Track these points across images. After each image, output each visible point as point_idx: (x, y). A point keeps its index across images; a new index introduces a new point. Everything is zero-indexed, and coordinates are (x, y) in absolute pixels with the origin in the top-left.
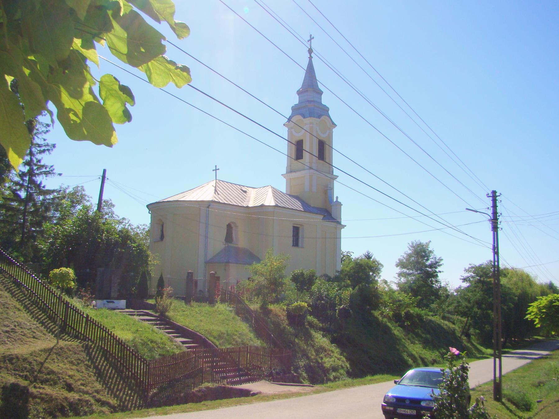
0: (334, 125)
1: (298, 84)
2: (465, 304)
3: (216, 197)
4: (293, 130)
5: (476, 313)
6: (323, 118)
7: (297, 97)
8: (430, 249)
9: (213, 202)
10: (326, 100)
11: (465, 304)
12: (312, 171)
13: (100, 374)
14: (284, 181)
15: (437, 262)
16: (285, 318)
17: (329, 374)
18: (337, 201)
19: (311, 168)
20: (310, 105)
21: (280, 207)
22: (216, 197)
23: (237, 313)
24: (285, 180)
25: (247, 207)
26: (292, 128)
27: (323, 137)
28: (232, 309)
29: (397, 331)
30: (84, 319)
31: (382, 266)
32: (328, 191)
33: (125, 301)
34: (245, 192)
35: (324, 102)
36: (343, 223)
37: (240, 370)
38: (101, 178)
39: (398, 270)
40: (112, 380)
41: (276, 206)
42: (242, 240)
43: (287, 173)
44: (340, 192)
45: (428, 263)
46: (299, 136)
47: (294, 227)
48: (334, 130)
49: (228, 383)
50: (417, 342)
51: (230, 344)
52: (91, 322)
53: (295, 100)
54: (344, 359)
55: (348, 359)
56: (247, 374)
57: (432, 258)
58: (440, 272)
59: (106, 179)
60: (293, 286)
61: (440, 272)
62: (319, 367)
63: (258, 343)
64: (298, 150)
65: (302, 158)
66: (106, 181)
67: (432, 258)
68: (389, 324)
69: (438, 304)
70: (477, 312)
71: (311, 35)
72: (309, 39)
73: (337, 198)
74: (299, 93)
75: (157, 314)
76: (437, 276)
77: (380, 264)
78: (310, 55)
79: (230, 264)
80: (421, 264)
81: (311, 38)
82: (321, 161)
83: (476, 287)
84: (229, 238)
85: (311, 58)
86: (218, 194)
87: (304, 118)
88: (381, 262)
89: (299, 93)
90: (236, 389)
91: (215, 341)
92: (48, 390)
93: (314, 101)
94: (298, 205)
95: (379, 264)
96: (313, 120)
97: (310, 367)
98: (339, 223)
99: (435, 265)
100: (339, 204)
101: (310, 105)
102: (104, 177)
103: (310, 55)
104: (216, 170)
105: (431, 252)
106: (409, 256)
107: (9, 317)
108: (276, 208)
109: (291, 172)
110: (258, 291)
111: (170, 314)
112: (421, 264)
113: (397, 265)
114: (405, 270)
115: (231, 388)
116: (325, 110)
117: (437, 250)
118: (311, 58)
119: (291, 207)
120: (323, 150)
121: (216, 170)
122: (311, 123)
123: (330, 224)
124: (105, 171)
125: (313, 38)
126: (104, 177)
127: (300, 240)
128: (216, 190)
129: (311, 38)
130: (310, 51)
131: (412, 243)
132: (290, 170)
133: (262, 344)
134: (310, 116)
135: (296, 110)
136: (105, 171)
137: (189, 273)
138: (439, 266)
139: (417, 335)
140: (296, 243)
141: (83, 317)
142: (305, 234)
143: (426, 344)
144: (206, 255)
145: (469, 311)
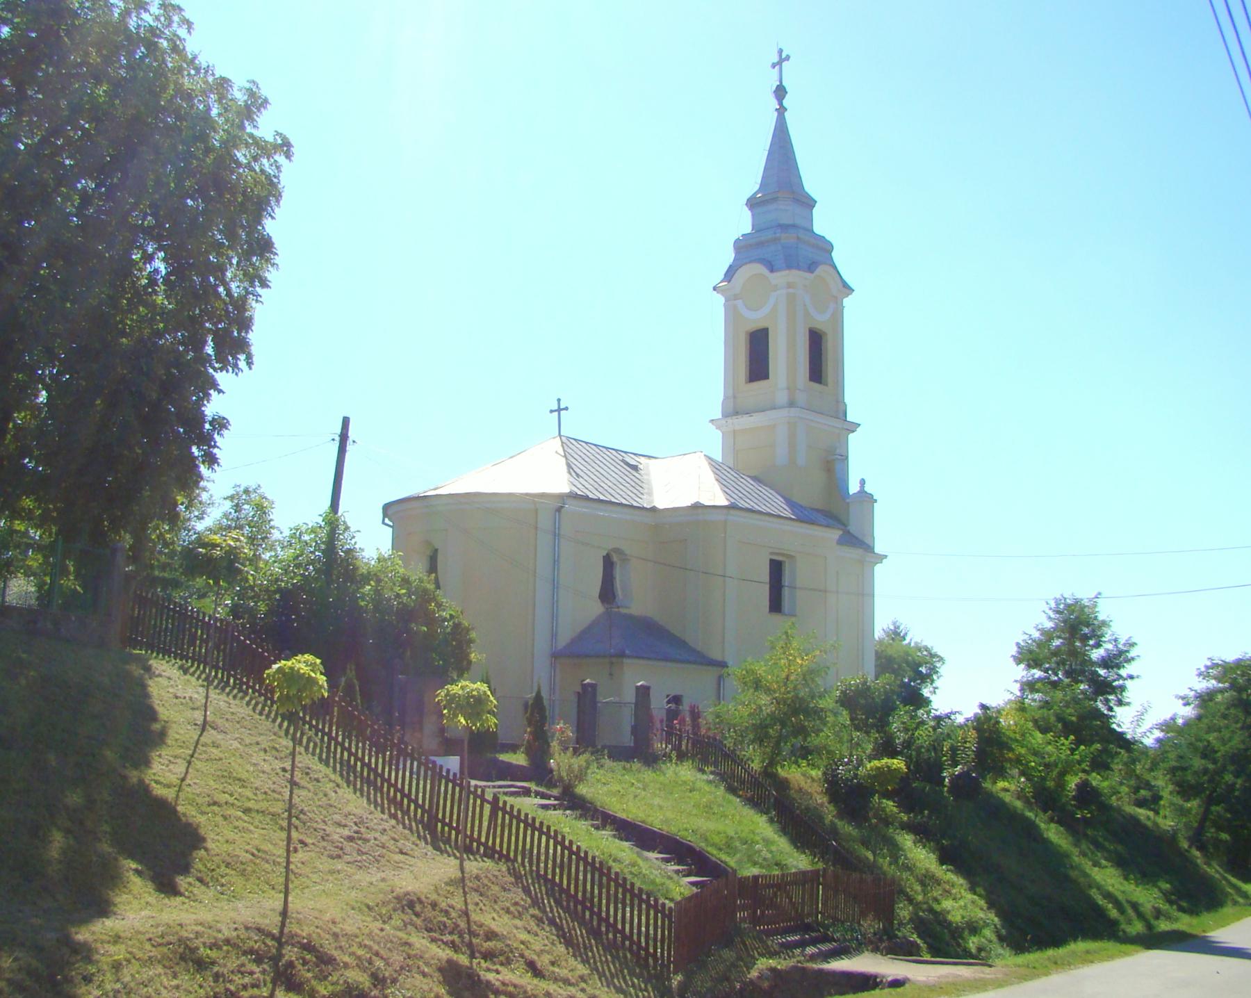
0: (847, 289)
1: (751, 183)
2: (1198, 763)
3: (576, 483)
4: (739, 303)
5: (1231, 787)
6: (821, 270)
7: (747, 215)
8: (1101, 617)
9: (573, 496)
10: (823, 223)
11: (1198, 763)
12: (794, 412)
13: (569, 942)
14: (717, 436)
15: (1121, 653)
16: (825, 799)
17: (963, 939)
18: (862, 492)
19: (792, 404)
20: (783, 237)
21: (741, 509)
22: (576, 483)
23: (732, 790)
24: (719, 434)
25: (654, 509)
26: (736, 297)
27: (821, 320)
28: (712, 777)
29: (1054, 834)
30: (487, 808)
31: (941, 659)
32: (833, 464)
33: (458, 758)
34: (635, 468)
35: (818, 228)
36: (879, 548)
37: (807, 928)
38: (337, 439)
39: (1020, 672)
40: (592, 951)
41: (733, 507)
42: (639, 598)
43: (726, 415)
44: (864, 466)
45: (1096, 654)
46: (756, 319)
47: (771, 561)
48: (846, 301)
49: (812, 958)
50: (1104, 862)
51: (755, 864)
52: (505, 812)
53: (743, 223)
54: (982, 903)
55: (991, 905)
56: (826, 939)
57: (1109, 641)
58: (1131, 677)
59: (350, 442)
60: (845, 717)
61: (1131, 677)
62: (940, 923)
63: (800, 862)
64: (755, 356)
65: (766, 377)
66: (349, 447)
67: (1109, 641)
68: (1030, 815)
69: (1125, 764)
70: (1234, 784)
71: (780, 51)
72: (776, 60)
73: (863, 482)
74: (752, 203)
75: (555, 792)
76: (1122, 688)
77: (936, 655)
78: (781, 104)
79: (626, 661)
80: (1074, 657)
81: (782, 60)
82: (816, 386)
83: (1225, 716)
84: (607, 593)
85: (781, 110)
86: (578, 475)
87: (772, 271)
88: (937, 649)
89: (752, 203)
90: (833, 974)
91: (724, 857)
92: (507, 975)
93: (794, 226)
94: (777, 505)
95: (932, 656)
96: (796, 276)
97: (921, 920)
98: (869, 548)
99: (1114, 661)
100: (866, 499)
101: (783, 237)
102: (344, 437)
103: (781, 104)
104: (559, 410)
105: (1104, 623)
106: (1048, 635)
107: (331, 802)
108: (732, 512)
109: (736, 413)
110: (760, 733)
111: (582, 790)
112: (1074, 657)
113: (1018, 660)
114: (1037, 673)
115: (821, 971)
116: (825, 248)
117: (1120, 622)
118: (781, 110)
119: (764, 509)
120: (820, 356)
121: (559, 410)
122: (789, 285)
123: (853, 553)
124: (346, 422)
125: (788, 58)
126: (344, 437)
127: (786, 592)
128: (569, 466)
129: (782, 60)
130: (780, 92)
131: (1057, 604)
132: (733, 409)
133: (813, 863)
134: (789, 267)
135: (746, 249)
136: (346, 422)
137: (584, 686)
138: (1128, 661)
139: (1098, 846)
140: (776, 605)
141: (483, 800)
142: (799, 576)
143: (1124, 864)
144: (554, 636)
145: (1210, 781)
